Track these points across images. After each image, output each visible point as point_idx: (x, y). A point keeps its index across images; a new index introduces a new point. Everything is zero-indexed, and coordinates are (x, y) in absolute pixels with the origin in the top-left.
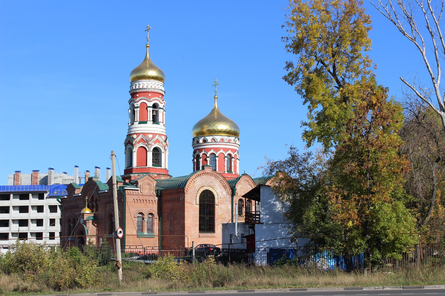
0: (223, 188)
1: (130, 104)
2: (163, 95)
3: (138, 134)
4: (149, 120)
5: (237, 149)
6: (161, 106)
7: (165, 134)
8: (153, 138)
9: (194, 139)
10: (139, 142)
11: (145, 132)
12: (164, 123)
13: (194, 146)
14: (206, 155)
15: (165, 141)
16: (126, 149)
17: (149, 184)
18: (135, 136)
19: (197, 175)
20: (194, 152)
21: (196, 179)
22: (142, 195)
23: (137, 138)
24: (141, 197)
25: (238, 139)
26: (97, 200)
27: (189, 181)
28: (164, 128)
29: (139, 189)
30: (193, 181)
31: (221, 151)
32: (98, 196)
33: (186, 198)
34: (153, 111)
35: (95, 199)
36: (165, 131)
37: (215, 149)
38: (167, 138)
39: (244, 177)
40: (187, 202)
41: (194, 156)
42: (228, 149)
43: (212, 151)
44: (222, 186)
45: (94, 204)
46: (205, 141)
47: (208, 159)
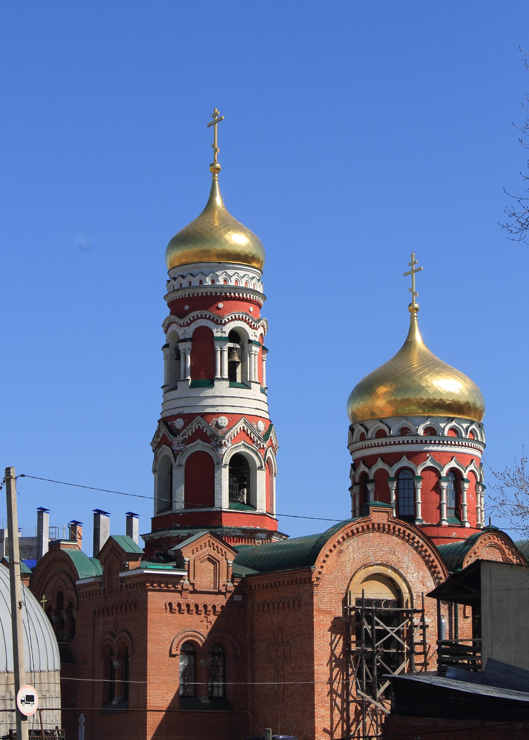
0: (426, 568)
1: (166, 332)
2: (259, 306)
3: (234, 417)
4: (218, 376)
5: (478, 454)
6: (254, 335)
7: (267, 416)
8: (230, 427)
9: (352, 429)
10: (235, 440)
11: (187, 411)
12: (265, 386)
13: (354, 446)
14: (438, 473)
15: (266, 436)
16: (156, 458)
17: (212, 560)
18: (224, 421)
19: (349, 531)
20: (354, 467)
21: (346, 544)
22: (194, 592)
23: (184, 427)
24: (192, 599)
25: (480, 426)
26: (71, 605)
27: (325, 551)
28: (264, 398)
29: (186, 574)
30: (335, 551)
31: (380, 465)
32: (73, 594)
33: (315, 600)
34: (230, 349)
35: (66, 604)
36: (265, 407)
37: (411, 455)
38: (271, 426)
39: (486, 536)
40: (319, 610)
41: (353, 477)
42: (398, 456)
43: (453, 464)
44: (422, 563)
45: (64, 616)
46: (431, 431)
47: (444, 485)
